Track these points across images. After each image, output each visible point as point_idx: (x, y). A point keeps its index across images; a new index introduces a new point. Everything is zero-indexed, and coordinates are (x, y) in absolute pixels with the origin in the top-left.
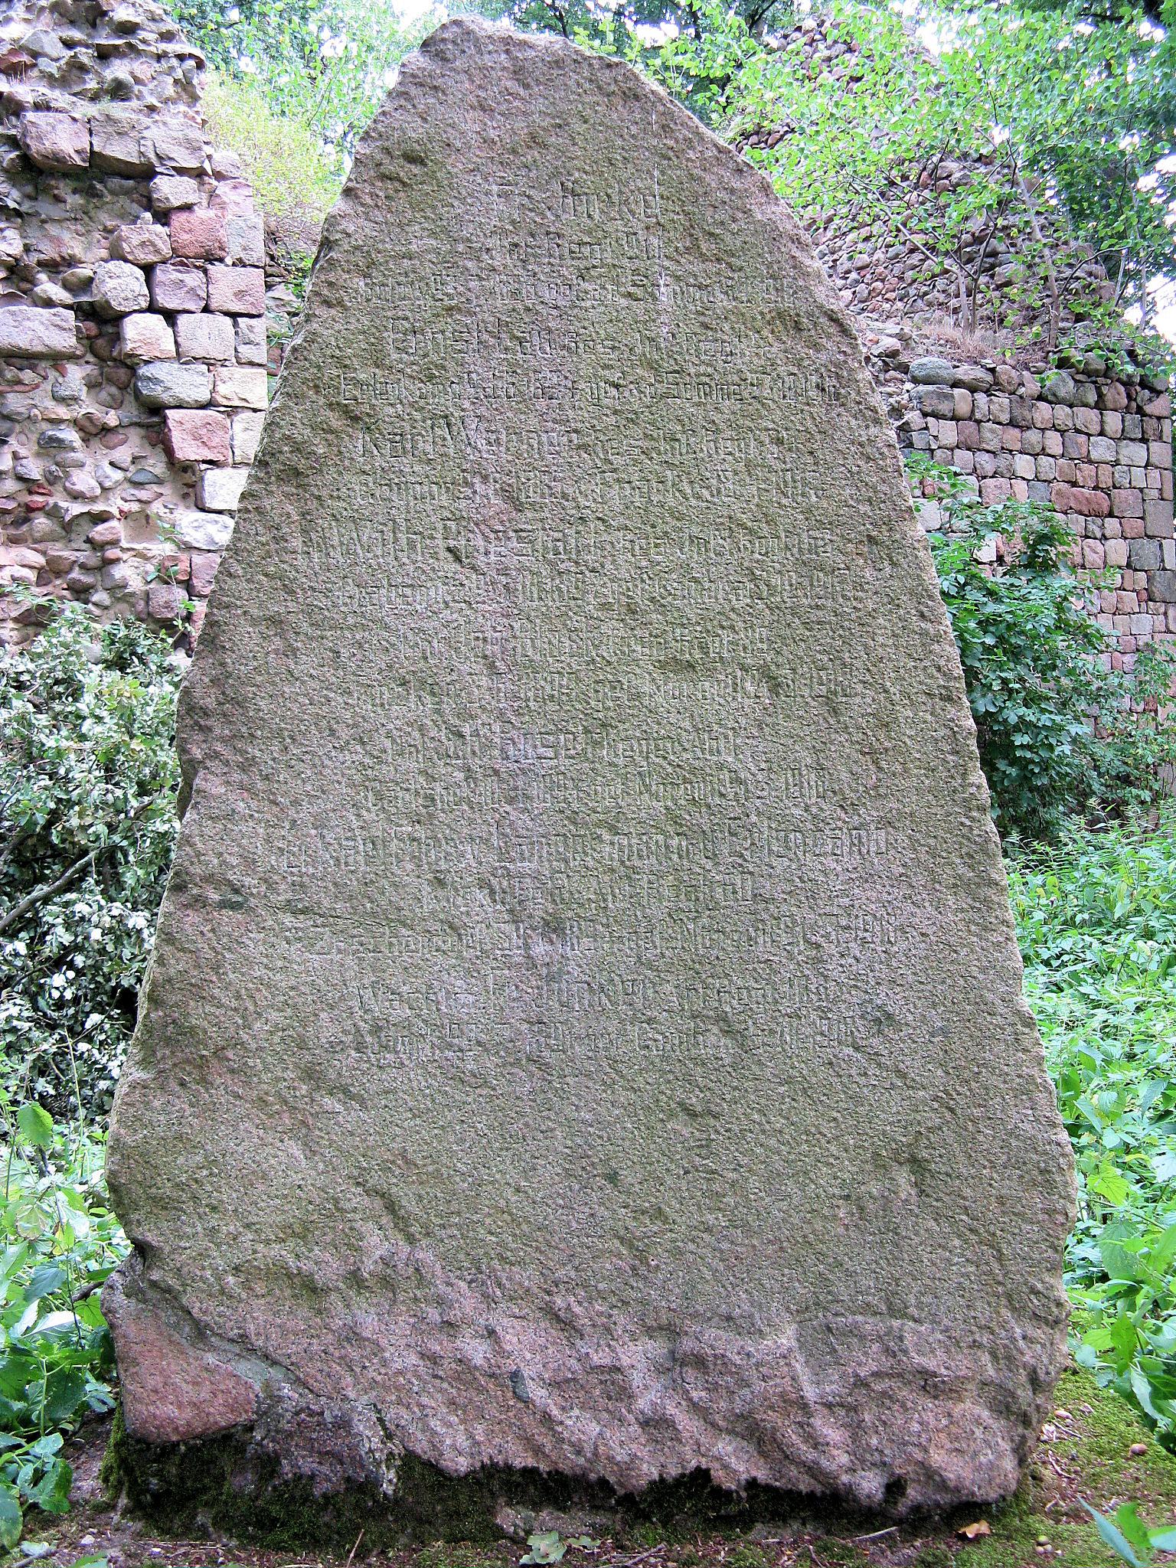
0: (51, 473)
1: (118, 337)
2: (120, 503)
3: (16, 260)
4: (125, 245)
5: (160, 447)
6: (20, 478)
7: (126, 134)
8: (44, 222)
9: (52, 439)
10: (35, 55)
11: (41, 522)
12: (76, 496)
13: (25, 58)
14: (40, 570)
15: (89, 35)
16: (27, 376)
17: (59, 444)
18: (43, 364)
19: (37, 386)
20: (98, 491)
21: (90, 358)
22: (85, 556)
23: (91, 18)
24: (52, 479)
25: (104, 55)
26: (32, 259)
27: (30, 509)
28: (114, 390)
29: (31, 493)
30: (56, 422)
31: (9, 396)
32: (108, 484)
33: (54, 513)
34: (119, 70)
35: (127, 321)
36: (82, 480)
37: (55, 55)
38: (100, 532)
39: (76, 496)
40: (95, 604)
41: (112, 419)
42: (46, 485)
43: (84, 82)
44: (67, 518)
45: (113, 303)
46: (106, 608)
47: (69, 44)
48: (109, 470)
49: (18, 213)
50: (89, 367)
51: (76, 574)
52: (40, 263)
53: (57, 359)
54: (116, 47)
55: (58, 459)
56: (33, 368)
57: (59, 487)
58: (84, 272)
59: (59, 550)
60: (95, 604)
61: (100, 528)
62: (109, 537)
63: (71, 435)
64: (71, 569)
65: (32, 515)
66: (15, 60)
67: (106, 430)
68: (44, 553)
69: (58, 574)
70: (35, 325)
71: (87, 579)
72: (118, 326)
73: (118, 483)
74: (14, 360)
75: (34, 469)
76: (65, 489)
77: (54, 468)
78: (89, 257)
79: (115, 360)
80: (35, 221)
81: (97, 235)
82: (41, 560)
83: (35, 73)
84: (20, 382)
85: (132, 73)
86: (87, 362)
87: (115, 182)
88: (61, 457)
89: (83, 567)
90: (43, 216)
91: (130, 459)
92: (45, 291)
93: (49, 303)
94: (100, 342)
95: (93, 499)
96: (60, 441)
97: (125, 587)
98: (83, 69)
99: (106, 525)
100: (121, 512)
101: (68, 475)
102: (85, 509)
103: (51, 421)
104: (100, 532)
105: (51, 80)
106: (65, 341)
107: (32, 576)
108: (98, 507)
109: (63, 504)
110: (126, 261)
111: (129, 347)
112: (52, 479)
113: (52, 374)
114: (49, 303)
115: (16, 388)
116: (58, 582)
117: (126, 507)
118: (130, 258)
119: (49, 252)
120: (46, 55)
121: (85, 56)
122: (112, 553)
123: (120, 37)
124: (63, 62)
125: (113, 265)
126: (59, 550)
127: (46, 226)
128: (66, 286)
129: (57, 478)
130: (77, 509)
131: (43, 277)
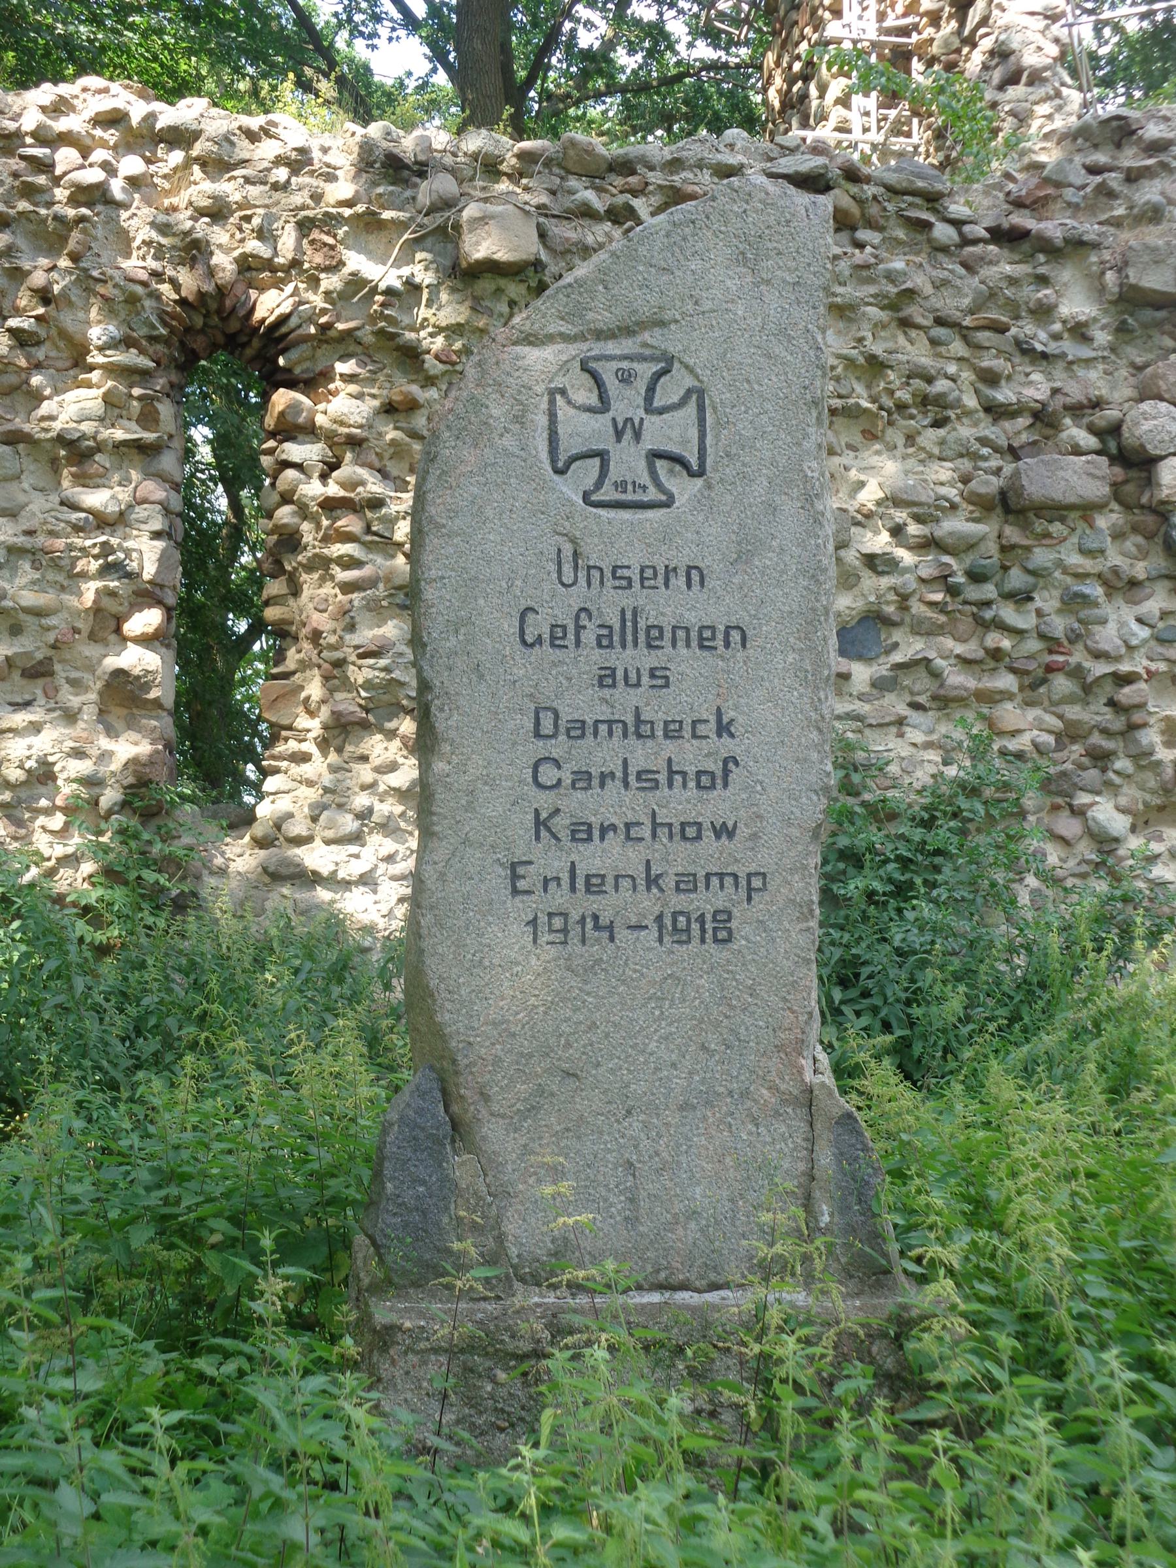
0: (1072, 630)
1: (1150, 481)
2: (1146, 662)
3: (1044, 405)
4: (1161, 383)
5: (952, 705)
6: (1042, 636)
7: (1163, 261)
8: (1071, 363)
9: (1077, 595)
10: (1058, 185)
11: (1062, 684)
12: (1098, 655)
13: (1050, 191)
14: (1058, 736)
15: (1113, 158)
16: (1056, 528)
17: (1086, 601)
18: (1074, 515)
19: (1065, 539)
20: (1123, 650)
21: (1115, 506)
22: (1106, 716)
23: (1116, 138)
24: (1074, 638)
25: (1133, 177)
26: (1060, 400)
27: (1050, 669)
28: (1139, 539)
29: (1051, 652)
30: (1081, 576)
31: (1036, 550)
32: (1134, 642)
33: (1077, 673)
34: (1150, 192)
35: (1162, 463)
36: (1107, 637)
37: (1079, 182)
38: (1126, 694)
39: (1098, 655)
40: (1117, 772)
41: (1140, 570)
42: (1066, 643)
43: (1112, 209)
44: (1089, 679)
45: (1149, 447)
46: (1129, 776)
47: (1093, 170)
48: (1135, 626)
49: (1044, 356)
50: (1114, 516)
51: (1096, 739)
52: (1067, 408)
53: (1087, 510)
54: (1147, 168)
55: (1082, 615)
56: (1062, 520)
57: (1080, 646)
58: (1112, 414)
59: (1074, 712)
60: (1117, 772)
61: (1127, 690)
62: (1137, 700)
63: (1096, 591)
64: (1090, 733)
65: (1050, 676)
66: (84, 211)
67: (1133, 583)
68: (1060, 717)
69: (1074, 739)
70: (1068, 474)
71: (1108, 744)
72: (1150, 472)
73: (1145, 641)
74: (1044, 512)
75: (1059, 625)
76: (1086, 647)
77: (1076, 625)
78: (1117, 396)
79: (1142, 507)
80: (1061, 365)
81: (1124, 372)
82: (1057, 724)
83: (1059, 205)
84: (1047, 535)
85: (1162, 193)
86: (1112, 511)
87: (1148, 314)
88: (1084, 613)
89: (1105, 732)
90: (1070, 358)
91: (1158, 614)
92: (1072, 437)
93: (1077, 451)
94: (1130, 488)
95: (1118, 659)
96: (1084, 597)
97: (1151, 754)
98: (1111, 194)
99: (1134, 687)
100: (1148, 672)
101: (1089, 634)
102: (1109, 669)
103: (1076, 576)
104: (1126, 694)
105: (1074, 207)
106: (1098, 490)
107: (1051, 739)
108: (1125, 668)
109: (1087, 664)
110: (1162, 399)
111: (1164, 493)
112: (1074, 638)
113: (1081, 525)
114: (1077, 451)
115: (1044, 542)
116: (1074, 748)
117: (1153, 666)
118: (1167, 396)
119: (1075, 393)
120: (1070, 185)
121: (1114, 180)
122: (1137, 718)
123: (1150, 157)
124: (1088, 190)
125: (1146, 406)
126: (1074, 712)
127: (1075, 367)
128: (1092, 430)
129: (1079, 636)
130: (1100, 669)
131: (1068, 421)
